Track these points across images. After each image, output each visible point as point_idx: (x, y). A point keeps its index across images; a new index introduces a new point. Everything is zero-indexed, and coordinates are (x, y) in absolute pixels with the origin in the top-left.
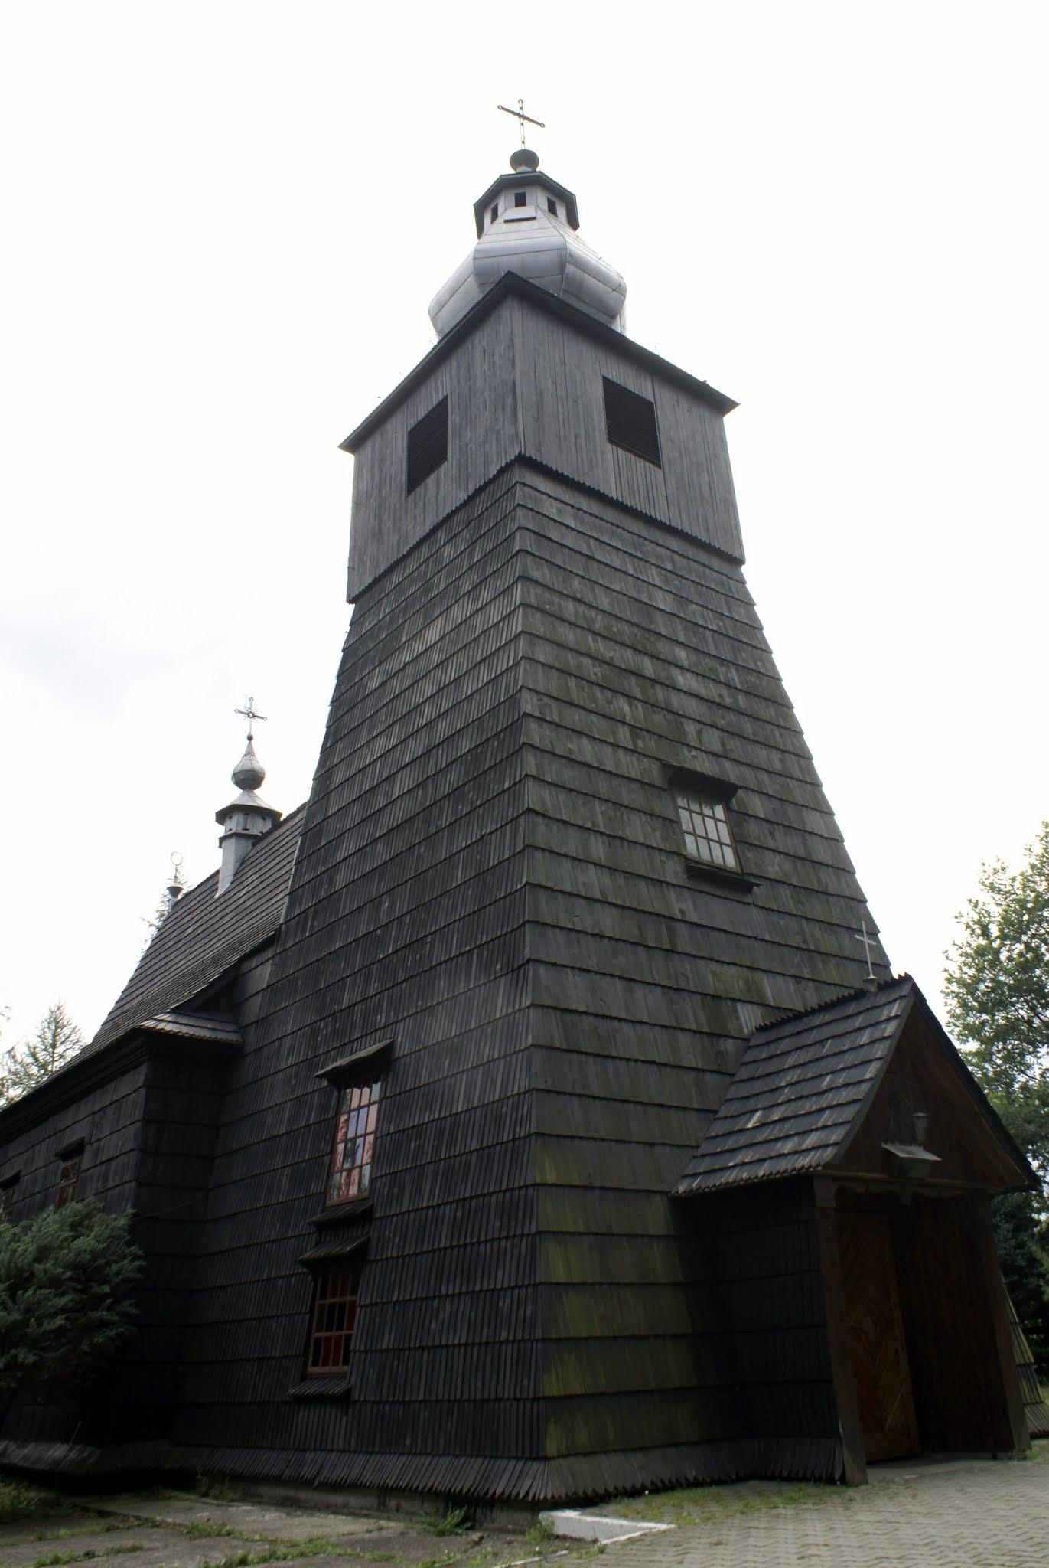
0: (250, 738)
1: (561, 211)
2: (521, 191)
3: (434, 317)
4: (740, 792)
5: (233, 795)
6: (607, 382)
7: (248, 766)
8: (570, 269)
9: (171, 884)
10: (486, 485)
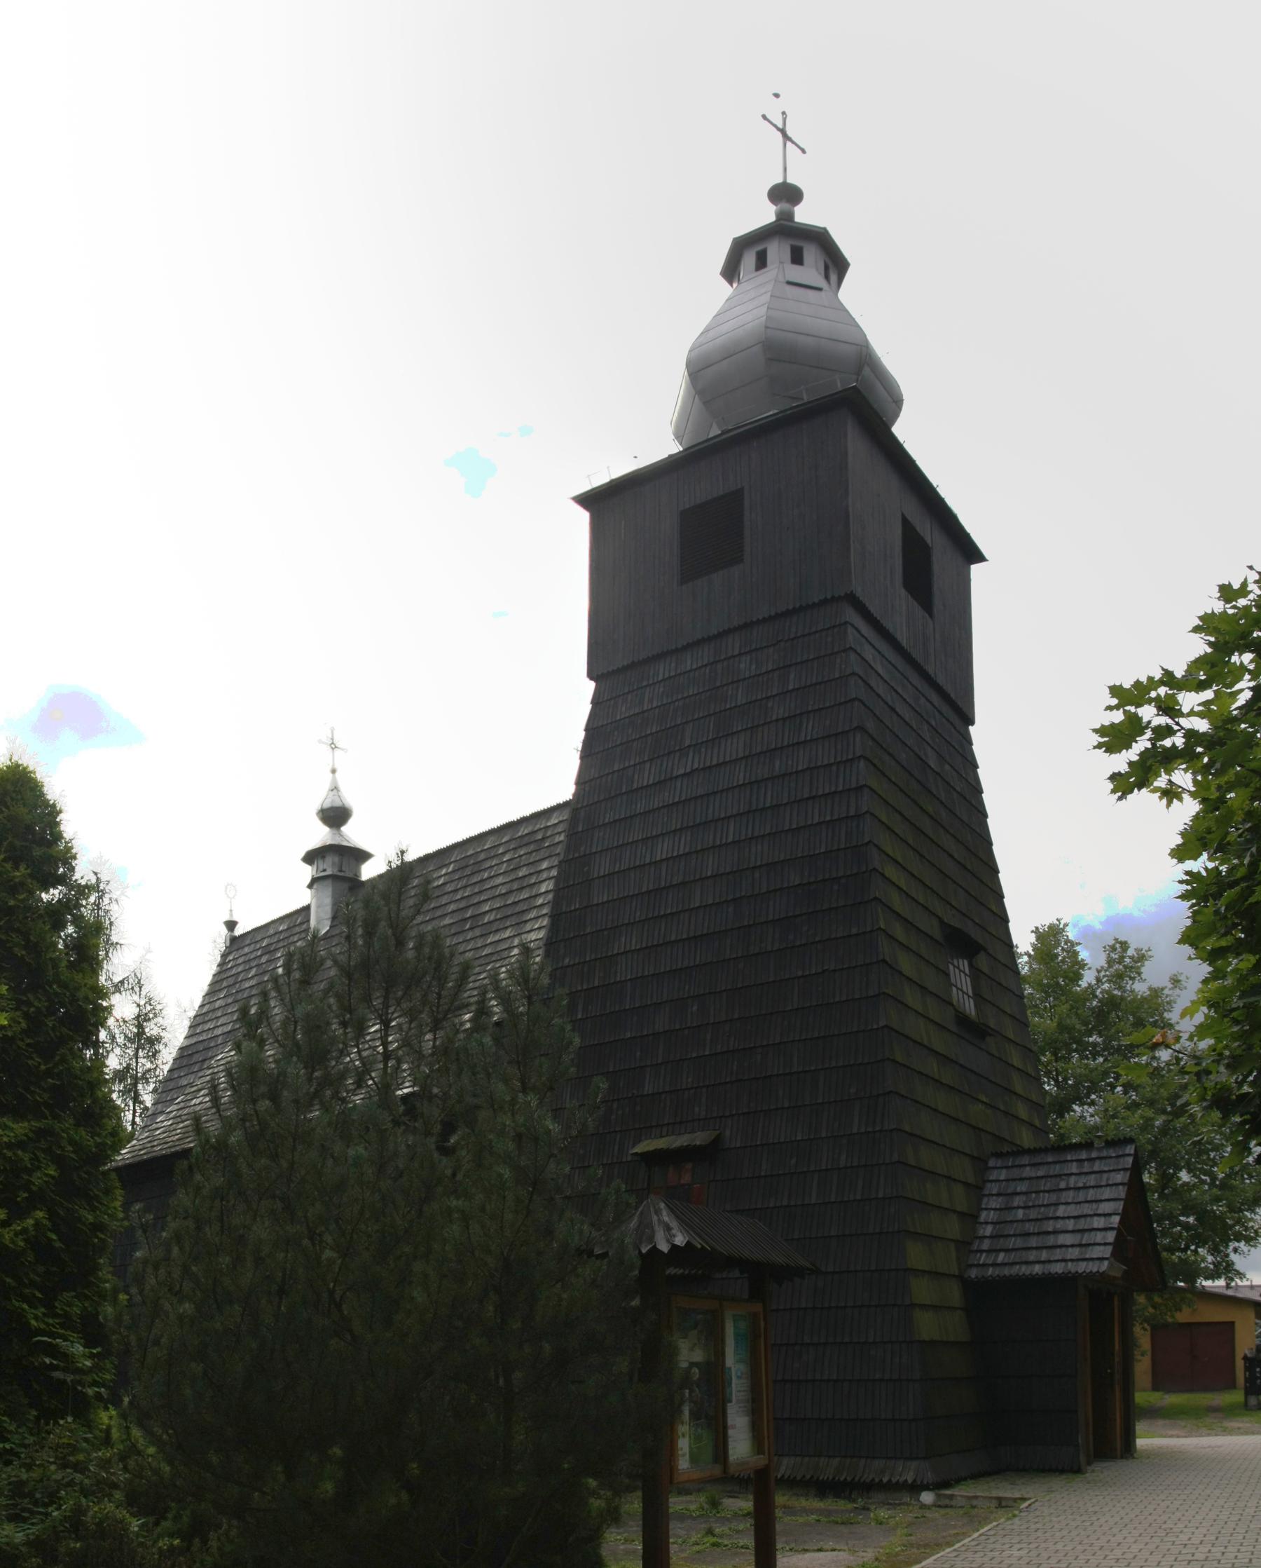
0: (334, 771)
1: (833, 277)
2: (798, 243)
3: (688, 366)
4: (982, 952)
5: (320, 835)
6: (905, 522)
7: (338, 804)
8: (867, 371)
9: (227, 918)
10: (802, 609)
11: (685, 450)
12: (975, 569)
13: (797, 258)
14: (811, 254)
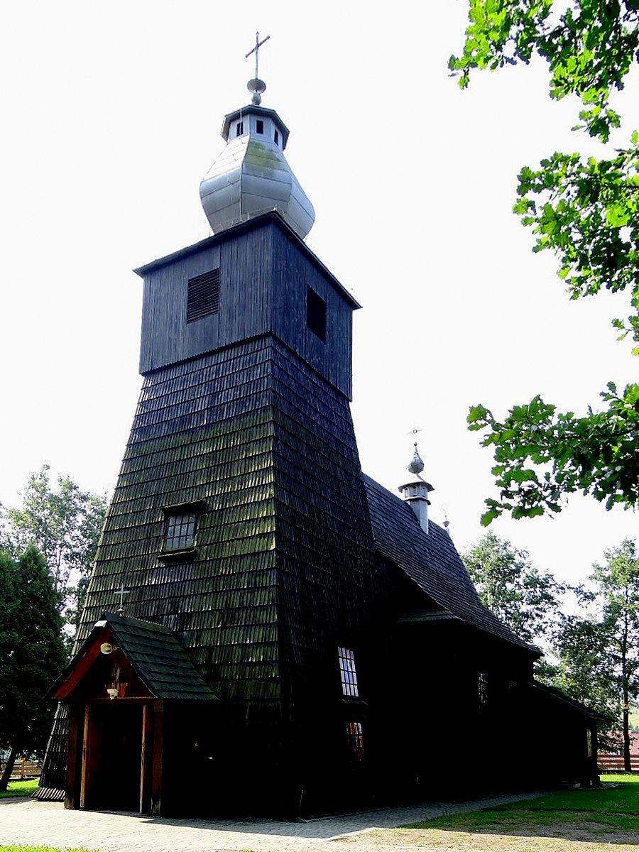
2: (261, 119)
11: (215, 235)
12: (355, 313)
13: (260, 129)
14: (270, 128)
